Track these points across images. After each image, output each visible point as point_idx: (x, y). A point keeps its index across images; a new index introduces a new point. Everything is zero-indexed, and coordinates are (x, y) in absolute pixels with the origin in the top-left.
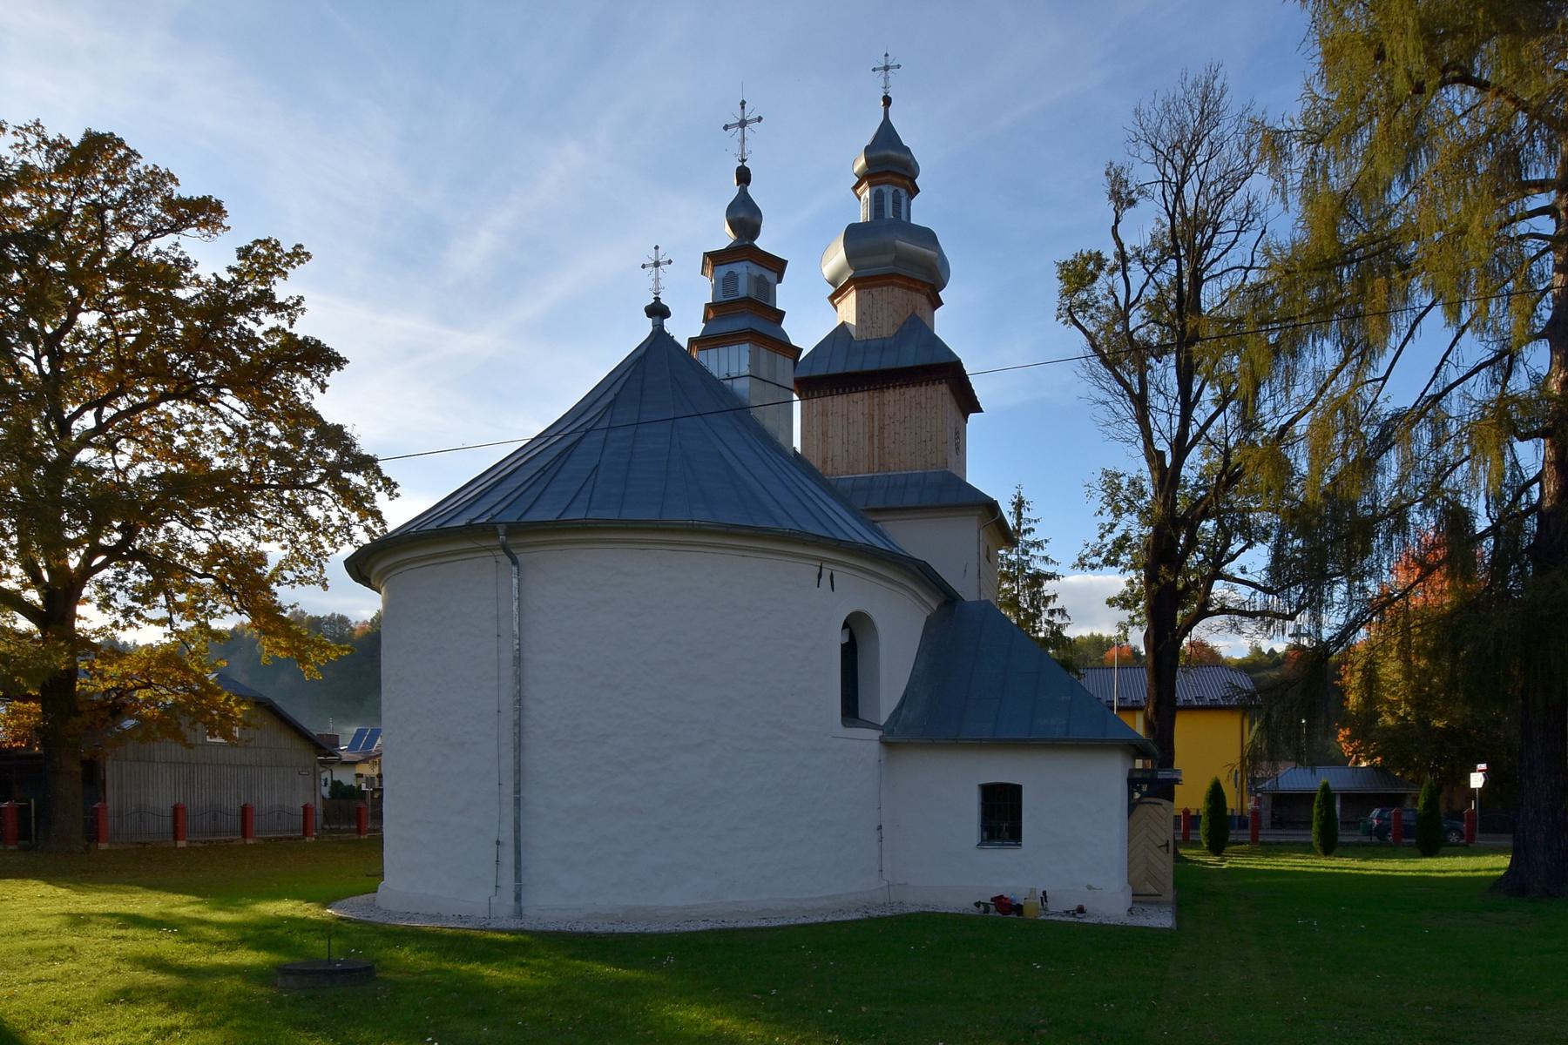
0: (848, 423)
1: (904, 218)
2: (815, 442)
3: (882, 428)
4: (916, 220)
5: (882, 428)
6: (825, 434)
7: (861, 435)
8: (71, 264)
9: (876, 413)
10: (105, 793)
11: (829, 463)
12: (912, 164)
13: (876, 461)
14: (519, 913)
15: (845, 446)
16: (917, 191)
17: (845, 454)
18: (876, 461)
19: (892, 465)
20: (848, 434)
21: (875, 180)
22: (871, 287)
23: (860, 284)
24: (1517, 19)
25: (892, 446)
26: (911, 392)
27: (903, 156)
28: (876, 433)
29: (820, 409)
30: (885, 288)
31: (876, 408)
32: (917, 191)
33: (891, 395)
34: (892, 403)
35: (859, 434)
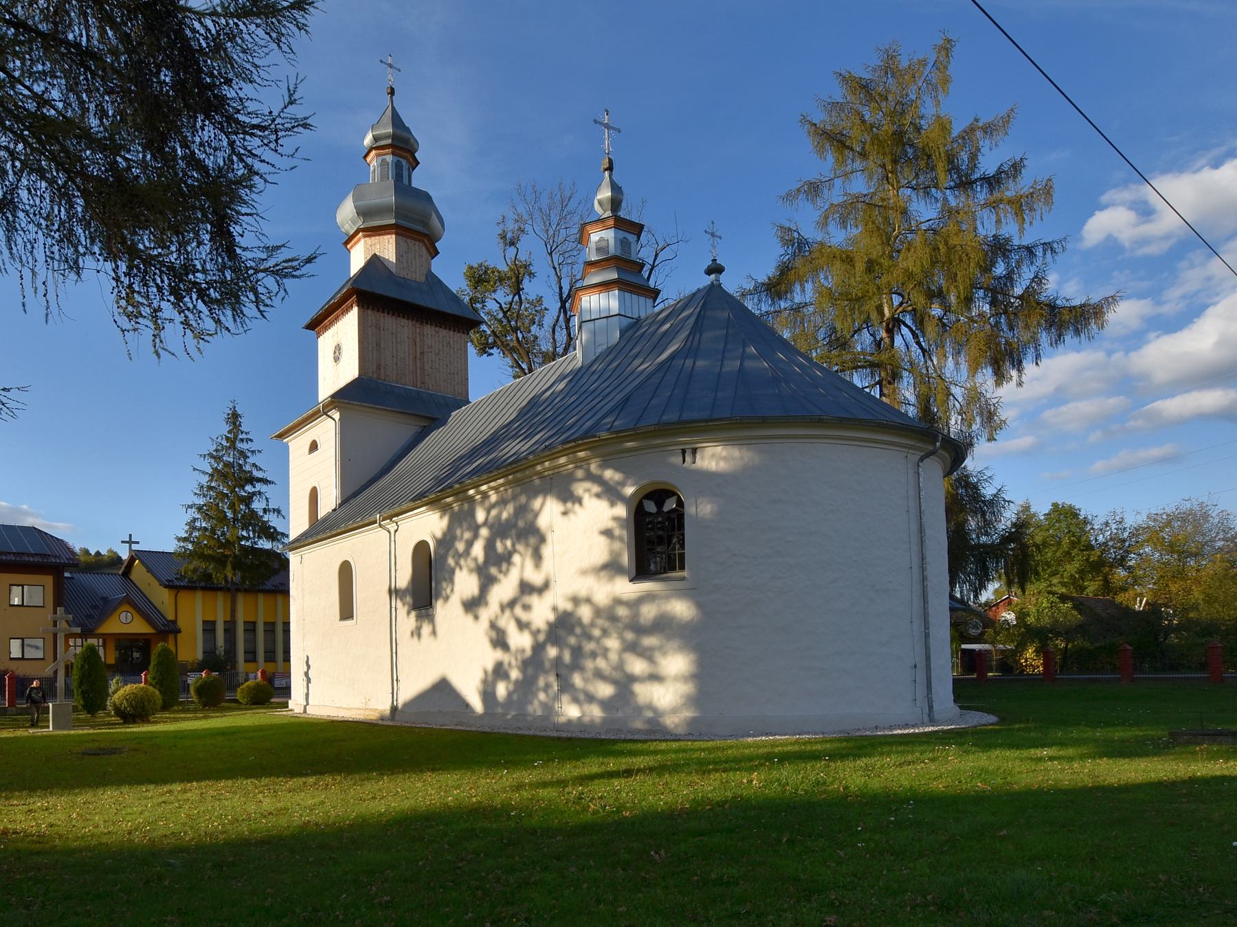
0: (397, 342)
1: (406, 181)
2: (371, 349)
3: (422, 353)
4: (415, 184)
5: (422, 353)
6: (378, 345)
7: (407, 354)
8: (1174, 611)
9: (418, 340)
10: (682, 546)
11: (382, 370)
12: (412, 140)
13: (419, 379)
14: (305, 711)
15: (395, 359)
16: (418, 163)
17: (395, 366)
18: (419, 379)
19: (430, 386)
20: (397, 351)
21: (398, 151)
22: (408, 237)
23: (399, 231)
24: (905, 374)
25: (430, 370)
26: (443, 333)
27: (405, 134)
28: (418, 357)
29: (374, 322)
30: (417, 243)
31: (418, 336)
32: (418, 163)
33: (429, 330)
34: (429, 336)
35: (405, 352)
